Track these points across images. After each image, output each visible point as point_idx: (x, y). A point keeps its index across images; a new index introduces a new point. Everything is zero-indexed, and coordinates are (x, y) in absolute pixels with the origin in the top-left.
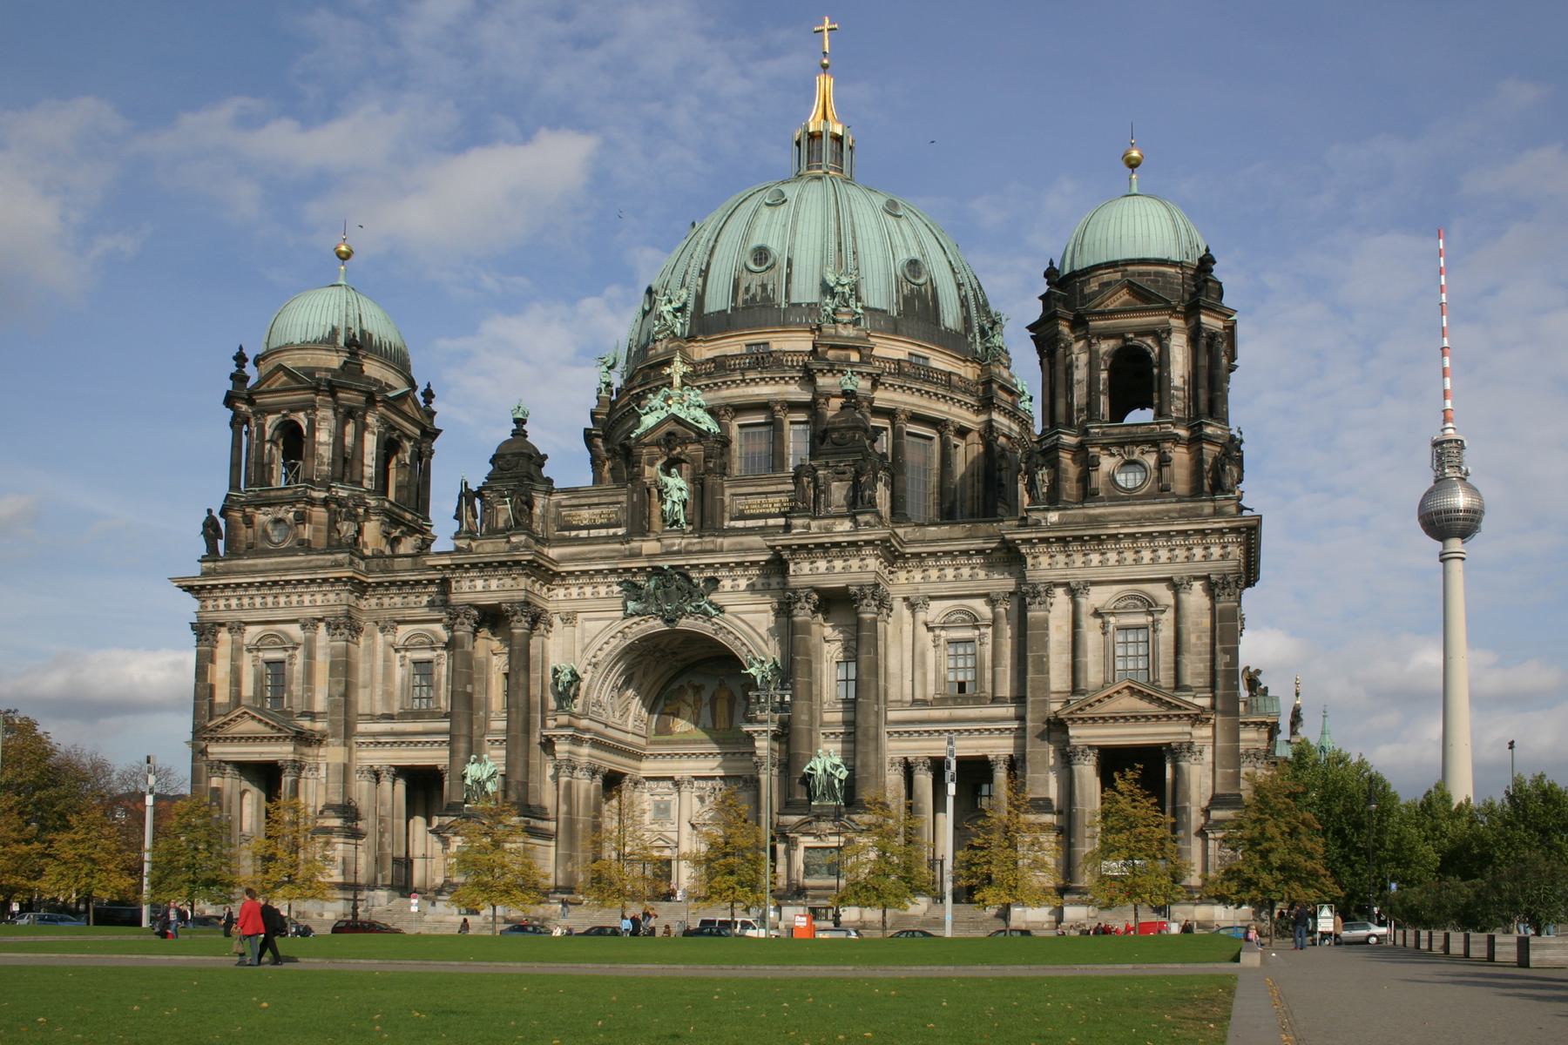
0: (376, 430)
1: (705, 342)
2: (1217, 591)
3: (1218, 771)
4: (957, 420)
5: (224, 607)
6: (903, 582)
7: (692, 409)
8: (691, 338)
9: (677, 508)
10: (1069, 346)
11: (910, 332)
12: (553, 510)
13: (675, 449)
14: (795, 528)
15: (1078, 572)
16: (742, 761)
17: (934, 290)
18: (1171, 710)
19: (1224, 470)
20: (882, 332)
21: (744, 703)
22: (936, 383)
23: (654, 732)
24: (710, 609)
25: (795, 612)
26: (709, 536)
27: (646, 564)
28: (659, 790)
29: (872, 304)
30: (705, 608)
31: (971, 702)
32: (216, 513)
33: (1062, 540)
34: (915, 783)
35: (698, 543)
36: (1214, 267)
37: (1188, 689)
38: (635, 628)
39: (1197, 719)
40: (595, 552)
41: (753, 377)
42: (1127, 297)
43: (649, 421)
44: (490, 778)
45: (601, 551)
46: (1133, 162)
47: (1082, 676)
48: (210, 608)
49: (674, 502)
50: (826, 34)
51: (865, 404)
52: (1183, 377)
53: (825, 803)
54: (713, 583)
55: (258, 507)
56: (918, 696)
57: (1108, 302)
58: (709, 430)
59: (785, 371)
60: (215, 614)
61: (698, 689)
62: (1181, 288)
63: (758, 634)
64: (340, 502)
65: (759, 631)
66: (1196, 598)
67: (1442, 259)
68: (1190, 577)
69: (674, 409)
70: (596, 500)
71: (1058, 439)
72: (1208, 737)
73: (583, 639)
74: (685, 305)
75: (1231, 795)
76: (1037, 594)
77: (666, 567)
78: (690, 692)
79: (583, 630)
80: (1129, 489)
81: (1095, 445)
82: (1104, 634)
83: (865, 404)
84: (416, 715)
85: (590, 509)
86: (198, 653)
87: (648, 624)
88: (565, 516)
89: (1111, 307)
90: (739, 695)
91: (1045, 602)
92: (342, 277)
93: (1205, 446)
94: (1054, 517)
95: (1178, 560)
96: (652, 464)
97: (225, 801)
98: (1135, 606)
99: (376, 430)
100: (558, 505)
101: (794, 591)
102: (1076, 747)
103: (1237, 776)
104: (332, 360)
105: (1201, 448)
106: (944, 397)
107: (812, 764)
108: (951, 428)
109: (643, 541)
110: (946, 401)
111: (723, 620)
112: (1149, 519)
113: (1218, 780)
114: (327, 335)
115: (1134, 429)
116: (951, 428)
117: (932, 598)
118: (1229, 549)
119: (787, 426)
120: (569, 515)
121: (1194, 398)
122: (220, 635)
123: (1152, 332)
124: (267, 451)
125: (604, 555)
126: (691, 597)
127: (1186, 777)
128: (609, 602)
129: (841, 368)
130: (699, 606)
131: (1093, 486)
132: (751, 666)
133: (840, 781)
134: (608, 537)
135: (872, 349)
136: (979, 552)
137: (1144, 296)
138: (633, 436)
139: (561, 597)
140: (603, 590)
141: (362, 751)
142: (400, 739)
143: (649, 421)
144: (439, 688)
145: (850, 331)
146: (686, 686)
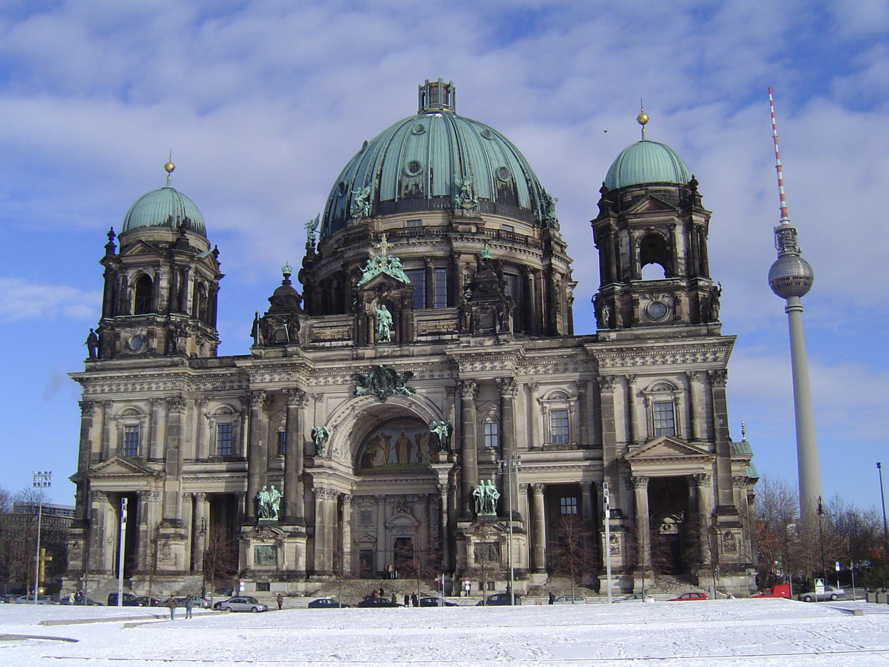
3: (720, 491)
4: (532, 264)
5: (99, 392)
6: (522, 377)
7: (394, 269)
8: (372, 216)
9: (386, 330)
10: (616, 235)
11: (503, 212)
13: (384, 293)
15: (630, 369)
16: (417, 485)
17: (515, 185)
18: (690, 454)
19: (712, 308)
20: (487, 213)
22: (520, 243)
23: (360, 466)
24: (408, 391)
27: (369, 364)
28: (364, 504)
29: (480, 196)
30: (405, 391)
31: (567, 448)
32: (94, 332)
35: (399, 350)
36: (697, 187)
37: (697, 440)
38: (361, 404)
40: (335, 356)
41: (414, 242)
44: (275, 501)
45: (339, 355)
47: (635, 432)
52: (684, 251)
58: (404, 282)
59: (398, 241)
60: (94, 396)
61: (388, 438)
62: (678, 198)
63: (436, 406)
64: (173, 323)
65: (437, 404)
66: (698, 387)
69: (383, 269)
70: (335, 324)
71: (613, 288)
74: (369, 196)
75: (729, 506)
77: (381, 366)
78: (383, 439)
82: (647, 406)
85: (331, 329)
86: (82, 419)
88: (316, 333)
89: (640, 211)
90: (414, 442)
91: (611, 387)
94: (613, 335)
95: (688, 361)
96: (370, 302)
97: (99, 518)
98: (665, 390)
100: (312, 327)
101: (463, 382)
103: (731, 494)
105: (698, 294)
106: (525, 251)
110: (525, 253)
112: (669, 337)
114: (166, 221)
115: (658, 283)
118: (718, 355)
120: (318, 333)
123: (659, 225)
124: (128, 293)
125: (341, 357)
127: (703, 495)
129: (468, 237)
130: (401, 390)
131: (636, 317)
133: (495, 500)
134: (343, 346)
135: (484, 224)
137: (659, 205)
138: (358, 285)
143: (367, 276)
146: (380, 436)
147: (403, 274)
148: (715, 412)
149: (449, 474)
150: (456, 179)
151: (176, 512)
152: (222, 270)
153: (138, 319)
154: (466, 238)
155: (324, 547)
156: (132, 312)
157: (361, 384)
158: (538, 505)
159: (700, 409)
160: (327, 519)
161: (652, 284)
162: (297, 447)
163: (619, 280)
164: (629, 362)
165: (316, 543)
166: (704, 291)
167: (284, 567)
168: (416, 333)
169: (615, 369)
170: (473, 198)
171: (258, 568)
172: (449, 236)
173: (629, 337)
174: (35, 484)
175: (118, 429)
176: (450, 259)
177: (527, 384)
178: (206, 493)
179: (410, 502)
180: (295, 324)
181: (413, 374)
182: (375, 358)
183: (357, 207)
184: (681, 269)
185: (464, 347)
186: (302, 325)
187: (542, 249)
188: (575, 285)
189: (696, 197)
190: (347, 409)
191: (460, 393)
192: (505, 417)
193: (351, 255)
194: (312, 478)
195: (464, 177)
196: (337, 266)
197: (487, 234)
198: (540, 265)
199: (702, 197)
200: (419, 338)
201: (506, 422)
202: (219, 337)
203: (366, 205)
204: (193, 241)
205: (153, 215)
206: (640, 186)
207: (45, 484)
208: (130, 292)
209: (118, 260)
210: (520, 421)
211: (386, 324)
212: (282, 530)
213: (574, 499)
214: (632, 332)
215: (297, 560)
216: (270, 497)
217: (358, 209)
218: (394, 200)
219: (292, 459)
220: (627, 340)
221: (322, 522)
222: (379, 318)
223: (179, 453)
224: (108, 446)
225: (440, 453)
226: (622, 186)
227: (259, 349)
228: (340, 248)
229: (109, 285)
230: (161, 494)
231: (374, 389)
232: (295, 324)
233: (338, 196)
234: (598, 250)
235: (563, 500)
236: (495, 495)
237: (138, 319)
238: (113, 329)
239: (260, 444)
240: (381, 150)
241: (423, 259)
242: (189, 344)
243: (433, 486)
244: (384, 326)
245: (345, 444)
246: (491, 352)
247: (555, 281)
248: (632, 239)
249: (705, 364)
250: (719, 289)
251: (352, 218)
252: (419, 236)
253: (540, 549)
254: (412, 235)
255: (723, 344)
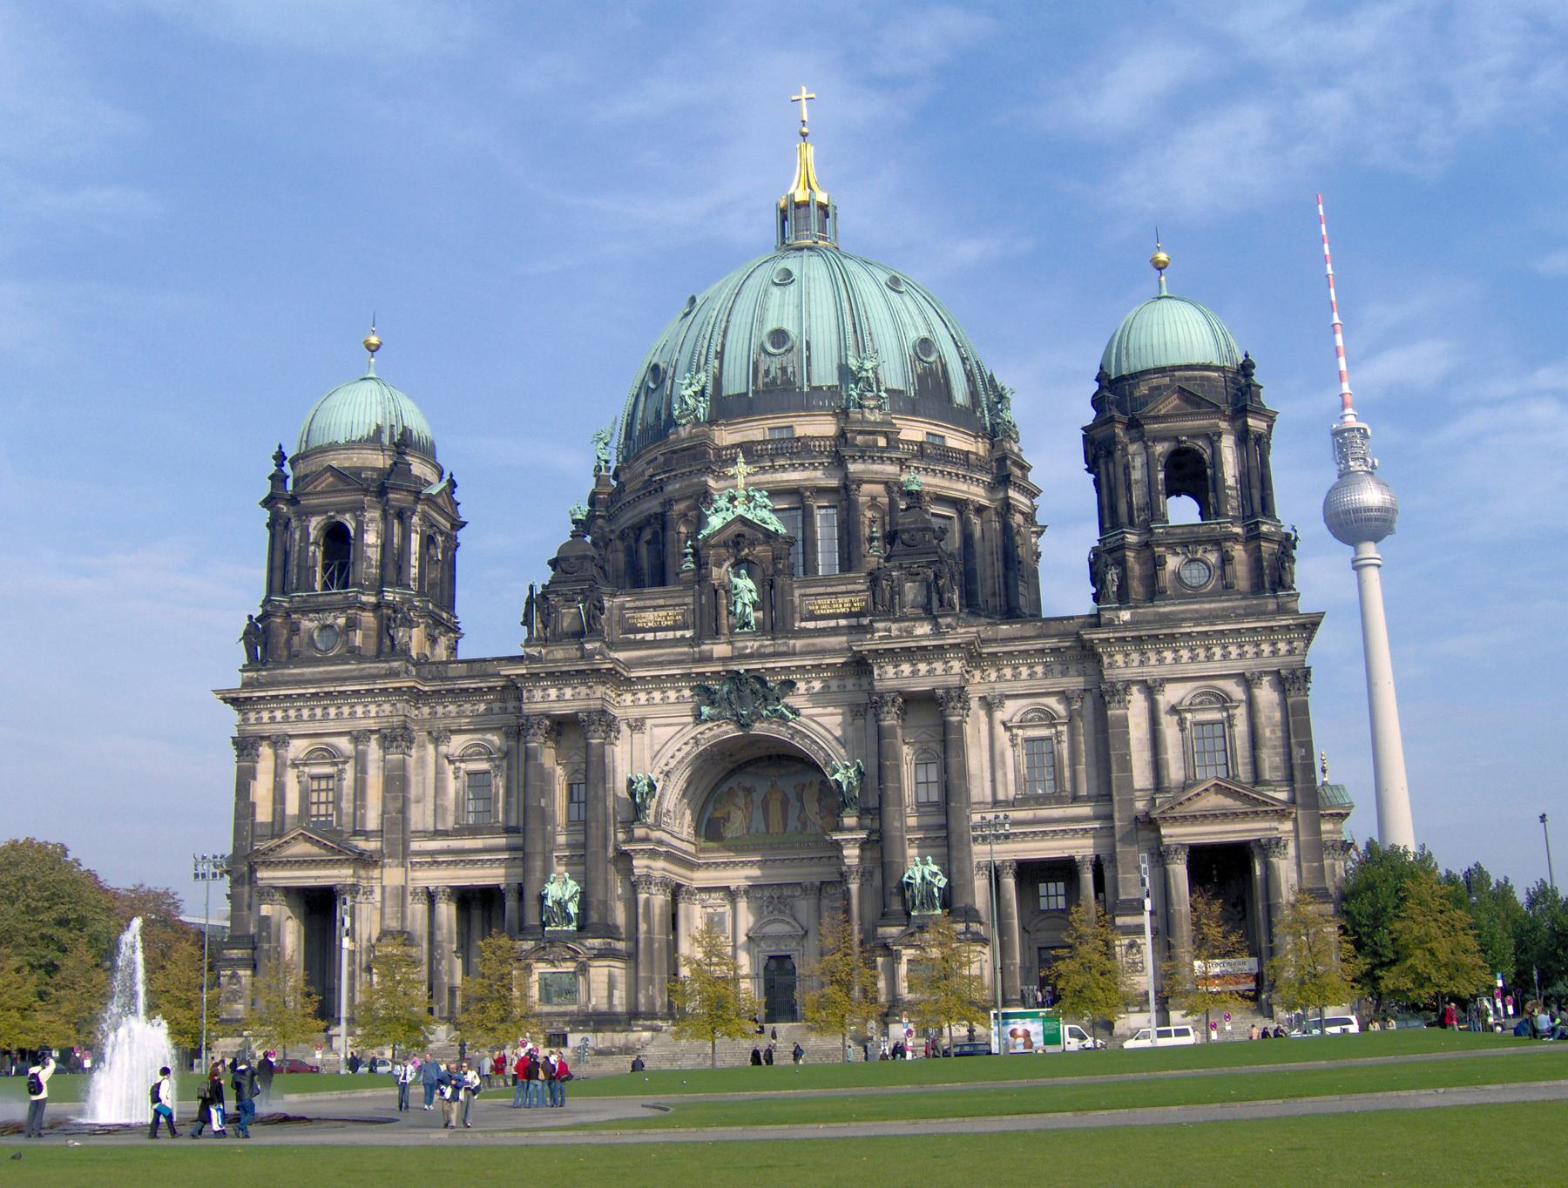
0: (419, 529)
1: (726, 425)
2: (1287, 686)
3: (1304, 865)
4: (976, 498)
5: (266, 720)
6: (980, 684)
7: (758, 509)
8: (712, 422)
12: (616, 612)
13: (743, 550)
14: (878, 631)
17: (944, 367)
18: (1258, 807)
19: (1284, 568)
21: (799, 804)
22: (956, 464)
24: (787, 713)
25: (882, 716)
26: (782, 638)
27: (721, 669)
28: (711, 901)
29: (889, 386)
33: (1139, 640)
34: (1002, 888)
35: (770, 645)
37: (1268, 783)
38: (708, 734)
39: (1282, 815)
41: (782, 463)
42: (1177, 402)
43: (715, 522)
44: (571, 898)
45: (669, 654)
46: (1161, 265)
47: (1165, 773)
48: (252, 721)
49: (745, 604)
50: (804, 102)
51: (895, 489)
52: (1235, 476)
53: (926, 913)
54: (791, 685)
55: (305, 613)
56: (582, 828)
57: (1161, 406)
59: (815, 457)
61: (748, 791)
64: (389, 605)
66: (1266, 694)
67: (1323, 226)
68: (1261, 672)
69: (740, 510)
70: (661, 602)
71: (1123, 539)
72: (1290, 832)
73: (652, 746)
76: (1115, 692)
77: (742, 671)
78: (741, 793)
79: (652, 737)
80: (1194, 587)
81: (1159, 545)
82: (1182, 730)
83: (895, 489)
84: (474, 831)
85: (655, 611)
86: (239, 769)
87: (722, 729)
90: (792, 795)
91: (1124, 700)
92: (372, 369)
93: (1262, 544)
94: (1125, 615)
95: (1248, 656)
96: (720, 566)
97: (273, 930)
98: (1211, 702)
99: (419, 529)
100: (622, 607)
101: (881, 695)
102: (1169, 846)
103: (1322, 867)
104: (377, 459)
105: (1259, 546)
106: (964, 477)
107: (910, 872)
108: (971, 507)
109: (714, 644)
110: (966, 480)
111: (800, 724)
112: (1217, 617)
113: (1304, 874)
115: (1196, 529)
116: (971, 507)
117: (1009, 697)
118: (1295, 644)
119: (816, 512)
120: (633, 618)
121: (1245, 496)
122: (261, 749)
125: (672, 658)
126: (766, 700)
128: (680, 707)
130: (776, 711)
131: (1161, 584)
132: (835, 771)
133: (939, 888)
135: (899, 433)
136: (1054, 651)
137: (1193, 400)
138: (700, 537)
139: (628, 703)
140: (672, 695)
141: (415, 871)
142: (461, 858)
143: (715, 522)
144: (497, 801)
145: (876, 416)
147: (774, 518)
148: (1292, 736)
149: (862, 849)
150: (850, 358)
151: (403, 918)
152: (464, 513)
153: (328, 598)
154: (869, 457)
155: (652, 971)
156: (318, 586)
157: (708, 702)
158: (1008, 896)
159: (1270, 733)
160: (656, 928)
161: (1186, 530)
162: (606, 808)
163: (1131, 523)
164: (1153, 657)
165: (641, 967)
166: (1271, 541)
167: (590, 1007)
168: (797, 616)
169: (1130, 671)
170: (879, 390)
171: (546, 1009)
172: (842, 454)
173: (1151, 618)
174: (196, 876)
175: (299, 782)
176: (843, 491)
177: (985, 697)
178: (450, 887)
179: (789, 897)
180: (597, 604)
181: (795, 684)
182: (731, 658)
183: (684, 407)
184: (1232, 505)
185: (881, 638)
186: (607, 604)
187: (992, 473)
188: (1042, 532)
189: (1253, 388)
190: (685, 744)
191: (876, 715)
192: (952, 753)
193: (677, 486)
194: (631, 859)
195: (862, 355)
196: (652, 505)
197: (903, 449)
198: (984, 498)
199: (1262, 387)
200: (803, 624)
201: (953, 761)
202: (459, 625)
203: (700, 402)
204: (418, 468)
205: (349, 423)
206: (1161, 370)
207: (214, 875)
208: (314, 553)
209: (293, 500)
210: (977, 759)
211: (747, 602)
212: (583, 945)
213: (1061, 885)
214: (1156, 609)
215: (610, 996)
216: (561, 888)
217: (687, 410)
218: (747, 393)
219: (597, 828)
220: (1149, 622)
221: (649, 931)
222: (734, 592)
223: (405, 821)
224: (283, 810)
225: (844, 814)
226: (1132, 371)
227: (537, 646)
228: (659, 474)
229: (278, 545)
230: (378, 891)
231: (732, 709)
232: (597, 604)
233: (649, 387)
234: (1093, 476)
235: (1042, 887)
236: (940, 880)
237: (328, 598)
238: (288, 615)
239: (543, 805)
240: (722, 311)
241: (795, 492)
242: (415, 639)
243: (833, 869)
244: (745, 604)
245: (680, 801)
246: (926, 647)
247: (1015, 525)
248: (1151, 458)
249: (1275, 660)
250: (1293, 538)
251: (677, 425)
252: (790, 454)
253: (1012, 968)
254: (778, 453)
255: (1303, 626)
